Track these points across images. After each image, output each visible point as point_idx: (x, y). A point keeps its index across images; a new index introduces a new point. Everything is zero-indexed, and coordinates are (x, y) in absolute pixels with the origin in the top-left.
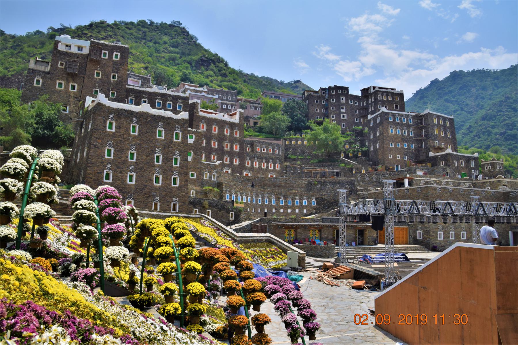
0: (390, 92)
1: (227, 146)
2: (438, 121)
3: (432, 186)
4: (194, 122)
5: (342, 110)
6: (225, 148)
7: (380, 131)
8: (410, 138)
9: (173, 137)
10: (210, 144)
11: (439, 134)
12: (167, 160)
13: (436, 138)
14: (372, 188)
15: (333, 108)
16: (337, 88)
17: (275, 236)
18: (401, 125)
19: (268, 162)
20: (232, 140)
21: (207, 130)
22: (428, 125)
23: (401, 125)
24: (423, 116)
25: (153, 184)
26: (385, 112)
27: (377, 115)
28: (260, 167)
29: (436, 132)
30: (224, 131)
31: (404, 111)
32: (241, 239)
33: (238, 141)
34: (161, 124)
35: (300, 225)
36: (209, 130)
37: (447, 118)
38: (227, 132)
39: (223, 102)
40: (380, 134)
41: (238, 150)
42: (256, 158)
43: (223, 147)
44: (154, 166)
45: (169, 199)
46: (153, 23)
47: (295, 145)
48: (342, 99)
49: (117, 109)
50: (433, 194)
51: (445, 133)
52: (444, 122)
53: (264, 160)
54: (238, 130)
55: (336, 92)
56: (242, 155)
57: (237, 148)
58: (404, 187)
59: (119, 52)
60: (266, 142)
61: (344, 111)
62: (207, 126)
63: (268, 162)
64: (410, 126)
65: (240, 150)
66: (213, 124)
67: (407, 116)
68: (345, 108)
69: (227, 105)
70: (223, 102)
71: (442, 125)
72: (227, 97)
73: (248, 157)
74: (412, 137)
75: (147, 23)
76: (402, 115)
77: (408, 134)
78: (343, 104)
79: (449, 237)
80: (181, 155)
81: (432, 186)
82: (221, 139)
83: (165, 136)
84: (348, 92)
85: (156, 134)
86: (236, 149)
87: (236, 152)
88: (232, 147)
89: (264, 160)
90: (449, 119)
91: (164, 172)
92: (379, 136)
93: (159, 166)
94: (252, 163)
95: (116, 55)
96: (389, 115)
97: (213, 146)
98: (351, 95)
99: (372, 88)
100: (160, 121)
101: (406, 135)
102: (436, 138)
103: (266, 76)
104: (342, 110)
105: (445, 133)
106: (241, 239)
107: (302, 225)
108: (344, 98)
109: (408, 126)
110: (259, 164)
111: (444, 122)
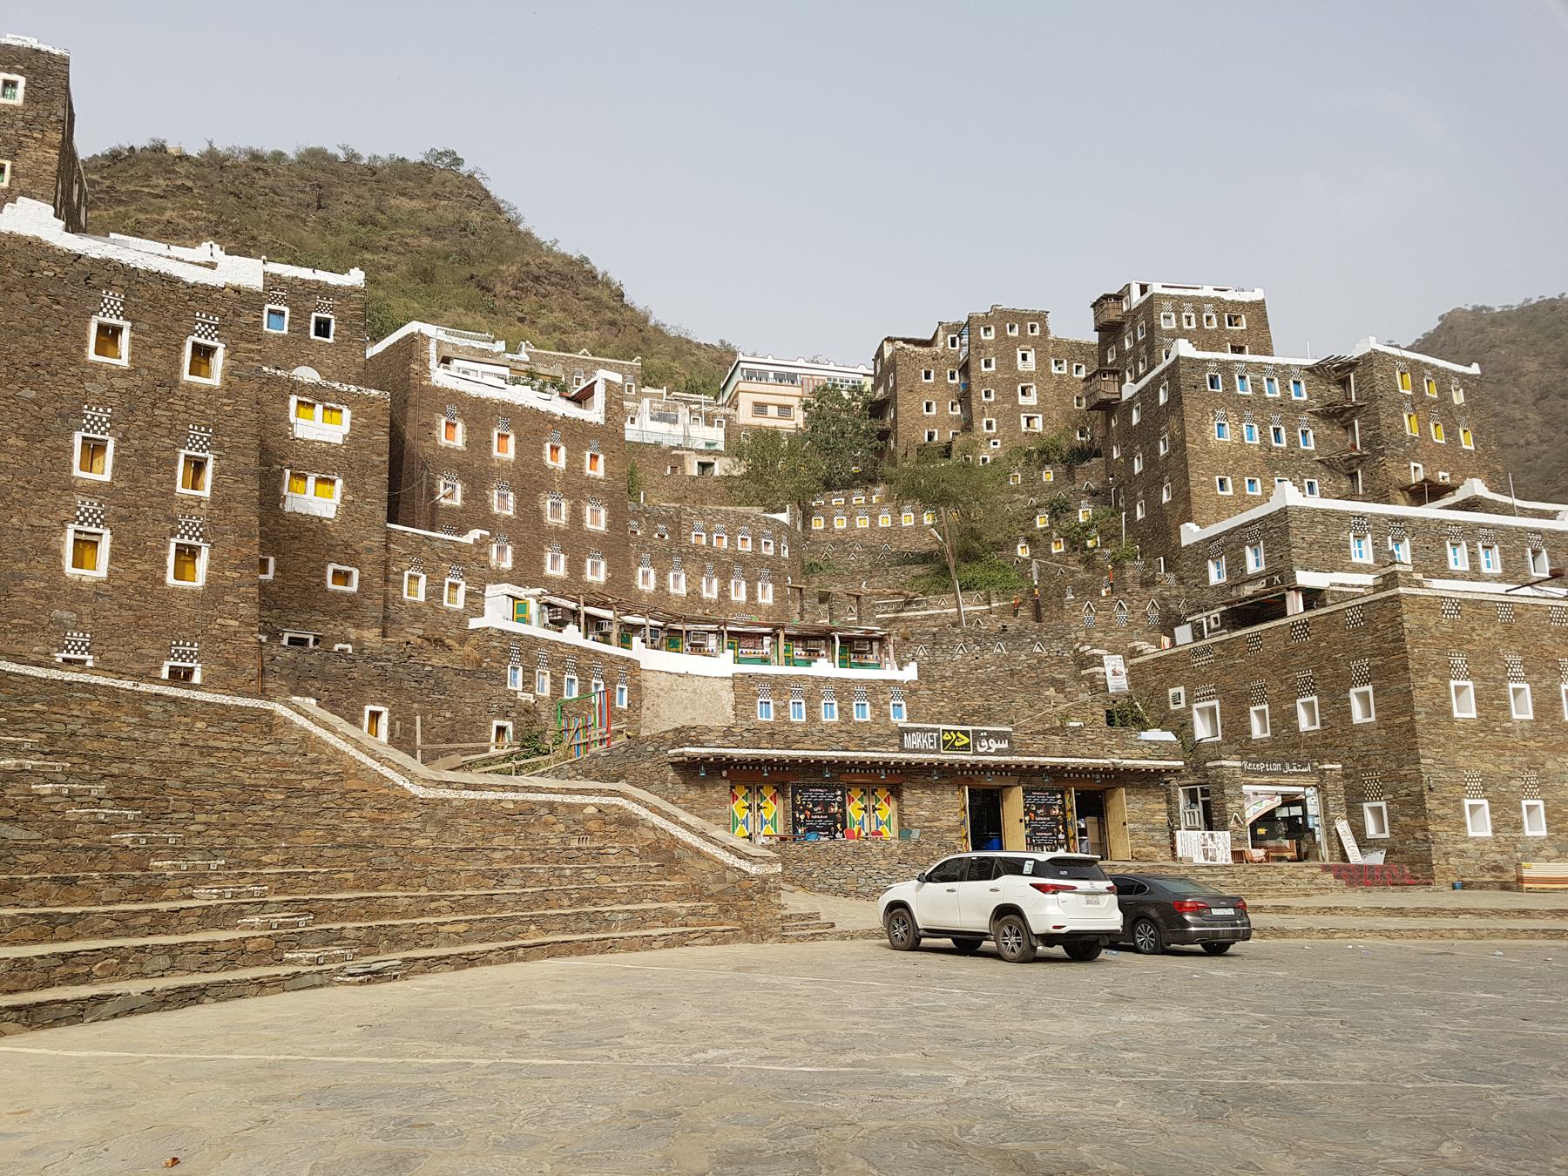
0: (1208, 300)
1: (556, 513)
2: (1417, 387)
3: (1419, 591)
4: (411, 413)
5: (1022, 400)
6: (549, 519)
7: (1172, 439)
8: (1299, 458)
9: (178, 364)
10: (485, 501)
11: (1424, 433)
12: (144, 465)
13: (1413, 449)
14: (1143, 645)
15: (987, 394)
16: (1004, 318)
18: (1257, 407)
19: (725, 577)
20: (577, 489)
21: (467, 444)
22: (1373, 399)
23: (1257, 407)
24: (1352, 365)
25: (61, 572)
26: (1190, 360)
27: (1158, 376)
28: (694, 595)
29: (1410, 427)
30: (540, 450)
31: (1268, 353)
34: (113, 298)
35: (794, 761)
36: (479, 443)
37: (1456, 374)
40: (1173, 449)
41: (602, 527)
42: (677, 559)
43: (539, 513)
44: (70, 487)
45: (149, 649)
46: (357, 157)
47: (843, 532)
48: (1024, 357)
50: (1423, 628)
51: (1451, 434)
52: (1443, 390)
55: (1001, 332)
56: (617, 548)
57: (596, 520)
58: (1284, 614)
59: (21, 73)
60: (727, 514)
61: (1031, 400)
62: (470, 430)
63: (725, 577)
64: (1297, 409)
65: (609, 526)
67: (1283, 371)
68: (1033, 391)
71: (1434, 402)
73: (646, 556)
74: (1309, 454)
75: (336, 157)
76: (1260, 367)
77: (1293, 442)
78: (1029, 376)
79: (1518, 826)
80: (220, 447)
81: (1419, 591)
82: (530, 481)
83: (132, 354)
84: (1045, 331)
85: (85, 343)
86: (595, 521)
87: (593, 536)
88: (576, 516)
90: (1462, 377)
91: (121, 518)
92: (1168, 457)
93: (93, 490)
94: (662, 577)
96: (1205, 370)
97: (496, 510)
98: (1058, 343)
99: (1136, 290)
100: (109, 285)
101: (1284, 445)
102: (1413, 449)
104: (1022, 400)
105: (1451, 434)
107: (806, 760)
108: (1031, 356)
109: (1289, 409)
110: (688, 581)
111: (1443, 390)
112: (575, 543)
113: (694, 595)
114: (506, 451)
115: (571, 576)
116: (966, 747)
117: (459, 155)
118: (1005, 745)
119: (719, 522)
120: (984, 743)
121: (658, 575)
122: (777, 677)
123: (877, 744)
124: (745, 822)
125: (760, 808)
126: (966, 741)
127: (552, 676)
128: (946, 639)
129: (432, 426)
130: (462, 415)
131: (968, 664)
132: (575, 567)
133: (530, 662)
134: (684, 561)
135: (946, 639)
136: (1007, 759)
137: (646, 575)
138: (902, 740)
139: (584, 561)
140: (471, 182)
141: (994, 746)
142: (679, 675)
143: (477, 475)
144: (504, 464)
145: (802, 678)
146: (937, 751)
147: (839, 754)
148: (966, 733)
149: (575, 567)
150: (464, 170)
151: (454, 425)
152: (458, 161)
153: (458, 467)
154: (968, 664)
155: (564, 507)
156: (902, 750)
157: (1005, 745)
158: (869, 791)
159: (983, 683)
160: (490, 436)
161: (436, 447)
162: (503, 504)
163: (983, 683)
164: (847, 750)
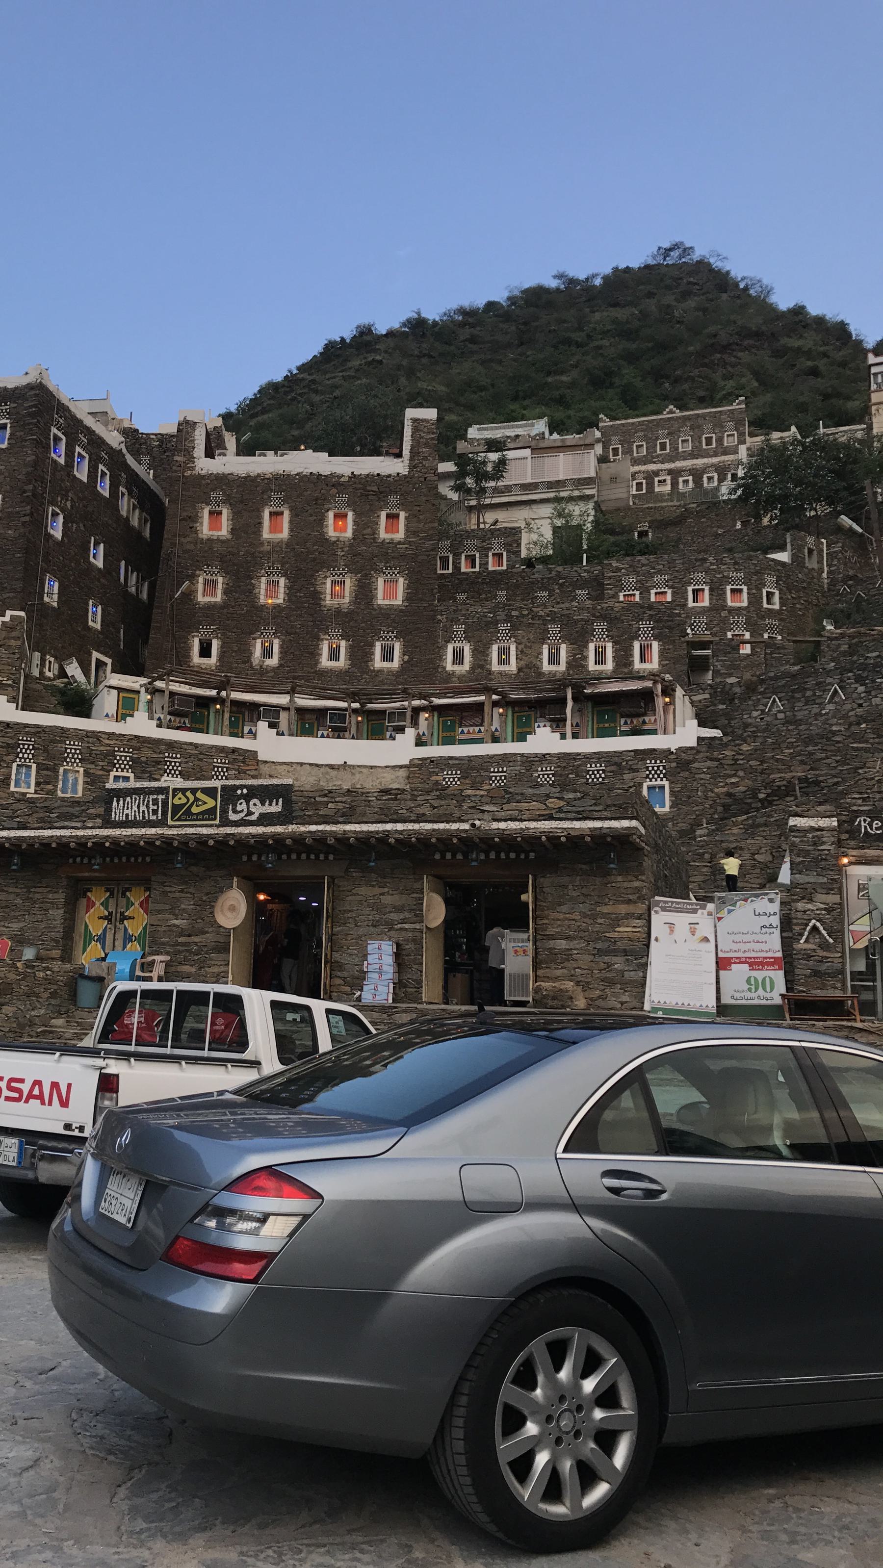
1: (337, 591)
17: (90, 664)
21: (233, 531)
28: (529, 669)
32: (66, 823)
33: (403, 556)
36: (246, 528)
38: (340, 528)
39: (679, 464)
49: (486, 1076)
53: (554, 629)
54: (403, 506)
62: (236, 516)
66: (265, 503)
69: (697, 474)
70: (679, 464)
72: (697, 439)
73: (459, 628)
87: (386, 613)
89: (554, 629)
95: (684, 481)
103: (386, 321)
106: (66, 823)
110: (520, 654)
112: (362, 623)
113: (529, 669)
114: (277, 529)
115: (353, 665)
116: (210, 813)
117: (688, 245)
118: (276, 808)
119: (660, 572)
120: (242, 806)
121: (475, 652)
122: (470, 759)
123: (70, 817)
124: (102, 939)
125: (124, 918)
126: (211, 803)
127: (87, 773)
128: (811, 682)
129: (194, 518)
130: (228, 501)
131: (846, 717)
132: (360, 655)
133: (50, 757)
134: (514, 628)
135: (811, 682)
136: (279, 829)
137: (504, 652)
138: (109, 810)
139: (372, 645)
140: (702, 265)
141: (258, 809)
142: (332, 767)
143: (241, 560)
144: (276, 546)
145: (506, 759)
146: (162, 823)
147: (13, 834)
148: (211, 792)
149: (360, 655)
150: (696, 256)
151: (220, 513)
152: (687, 251)
153: (222, 559)
154: (846, 717)
155: (349, 583)
156: (108, 823)
157: (276, 808)
158: (117, 887)
159: (809, 740)
160: (260, 517)
161: (198, 541)
162: (272, 592)
163: (809, 740)
164: (25, 828)
